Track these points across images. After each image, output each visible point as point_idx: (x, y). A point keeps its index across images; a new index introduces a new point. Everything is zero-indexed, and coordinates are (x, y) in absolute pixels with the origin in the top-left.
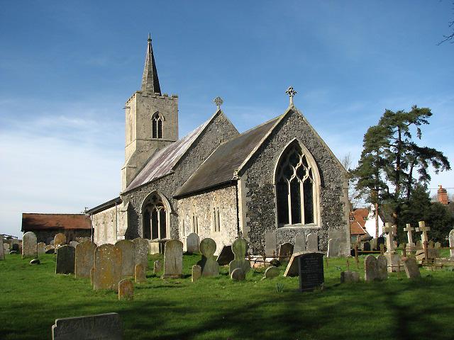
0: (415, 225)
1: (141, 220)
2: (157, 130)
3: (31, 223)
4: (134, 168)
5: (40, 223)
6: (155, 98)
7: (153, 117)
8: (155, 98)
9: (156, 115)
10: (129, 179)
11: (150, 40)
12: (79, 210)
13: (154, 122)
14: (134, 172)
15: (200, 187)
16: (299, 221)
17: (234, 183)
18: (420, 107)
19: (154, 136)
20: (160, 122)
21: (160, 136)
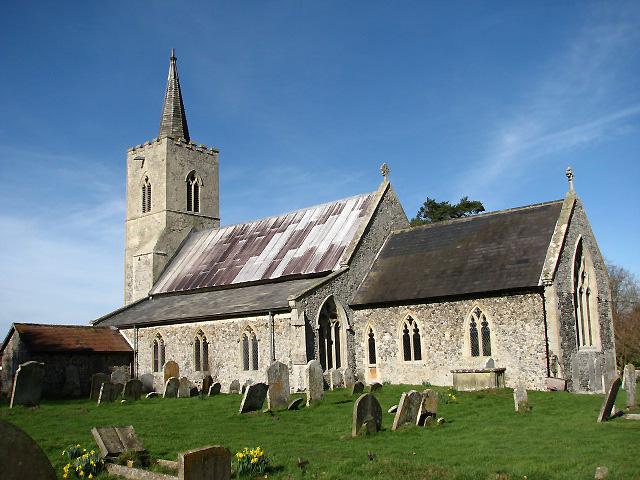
0: (175, 384)
1: (317, 340)
2: (192, 202)
3: (38, 341)
4: (164, 255)
5: (57, 342)
6: (181, 146)
7: (188, 179)
8: (181, 146)
9: (192, 176)
10: (264, 276)
11: (174, 59)
12: (84, 318)
13: (189, 187)
14: (163, 261)
15: (485, 290)
16: (410, 359)
17: (541, 290)
18: (471, 200)
19: (189, 209)
20: (196, 187)
21: (196, 210)
